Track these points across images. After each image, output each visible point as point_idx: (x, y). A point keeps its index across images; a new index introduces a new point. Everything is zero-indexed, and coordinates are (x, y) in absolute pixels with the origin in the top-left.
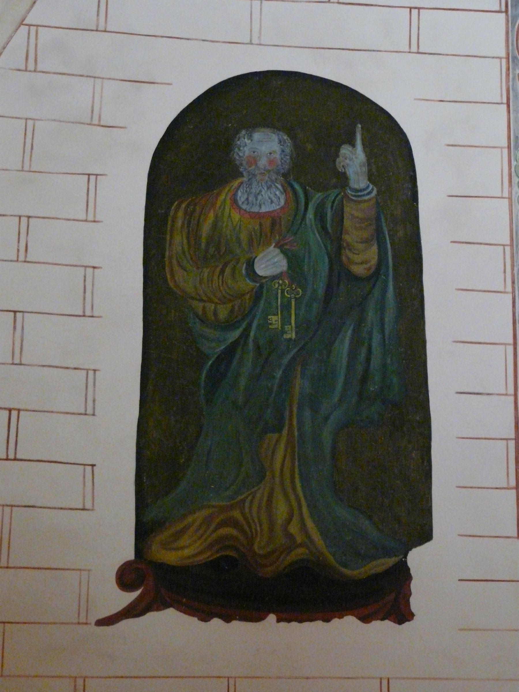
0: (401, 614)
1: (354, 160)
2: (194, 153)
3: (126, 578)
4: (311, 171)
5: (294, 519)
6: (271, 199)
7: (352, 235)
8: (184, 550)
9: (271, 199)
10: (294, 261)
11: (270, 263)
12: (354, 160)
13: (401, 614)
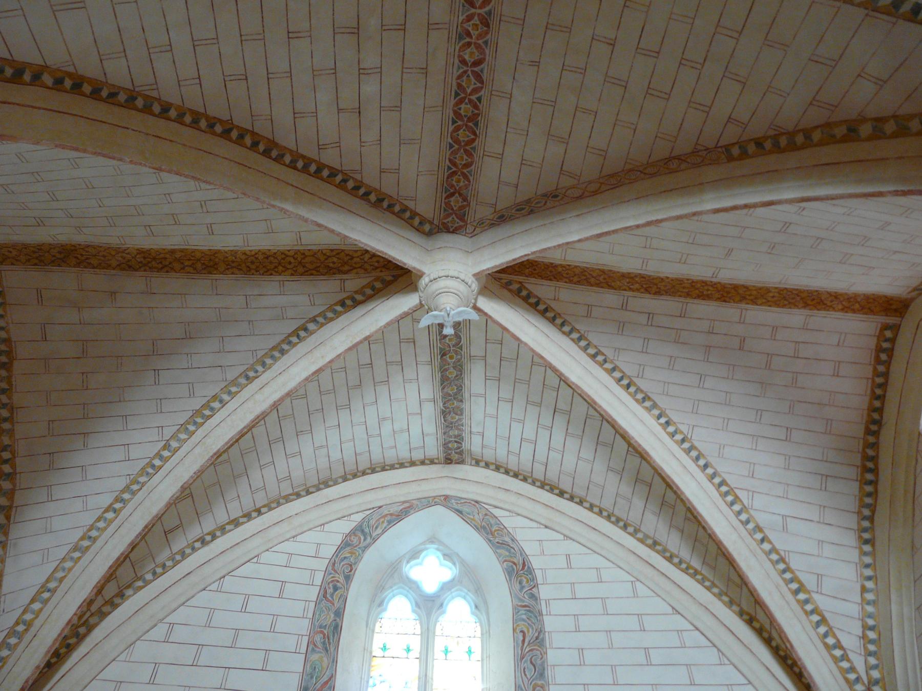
5: (528, 538)
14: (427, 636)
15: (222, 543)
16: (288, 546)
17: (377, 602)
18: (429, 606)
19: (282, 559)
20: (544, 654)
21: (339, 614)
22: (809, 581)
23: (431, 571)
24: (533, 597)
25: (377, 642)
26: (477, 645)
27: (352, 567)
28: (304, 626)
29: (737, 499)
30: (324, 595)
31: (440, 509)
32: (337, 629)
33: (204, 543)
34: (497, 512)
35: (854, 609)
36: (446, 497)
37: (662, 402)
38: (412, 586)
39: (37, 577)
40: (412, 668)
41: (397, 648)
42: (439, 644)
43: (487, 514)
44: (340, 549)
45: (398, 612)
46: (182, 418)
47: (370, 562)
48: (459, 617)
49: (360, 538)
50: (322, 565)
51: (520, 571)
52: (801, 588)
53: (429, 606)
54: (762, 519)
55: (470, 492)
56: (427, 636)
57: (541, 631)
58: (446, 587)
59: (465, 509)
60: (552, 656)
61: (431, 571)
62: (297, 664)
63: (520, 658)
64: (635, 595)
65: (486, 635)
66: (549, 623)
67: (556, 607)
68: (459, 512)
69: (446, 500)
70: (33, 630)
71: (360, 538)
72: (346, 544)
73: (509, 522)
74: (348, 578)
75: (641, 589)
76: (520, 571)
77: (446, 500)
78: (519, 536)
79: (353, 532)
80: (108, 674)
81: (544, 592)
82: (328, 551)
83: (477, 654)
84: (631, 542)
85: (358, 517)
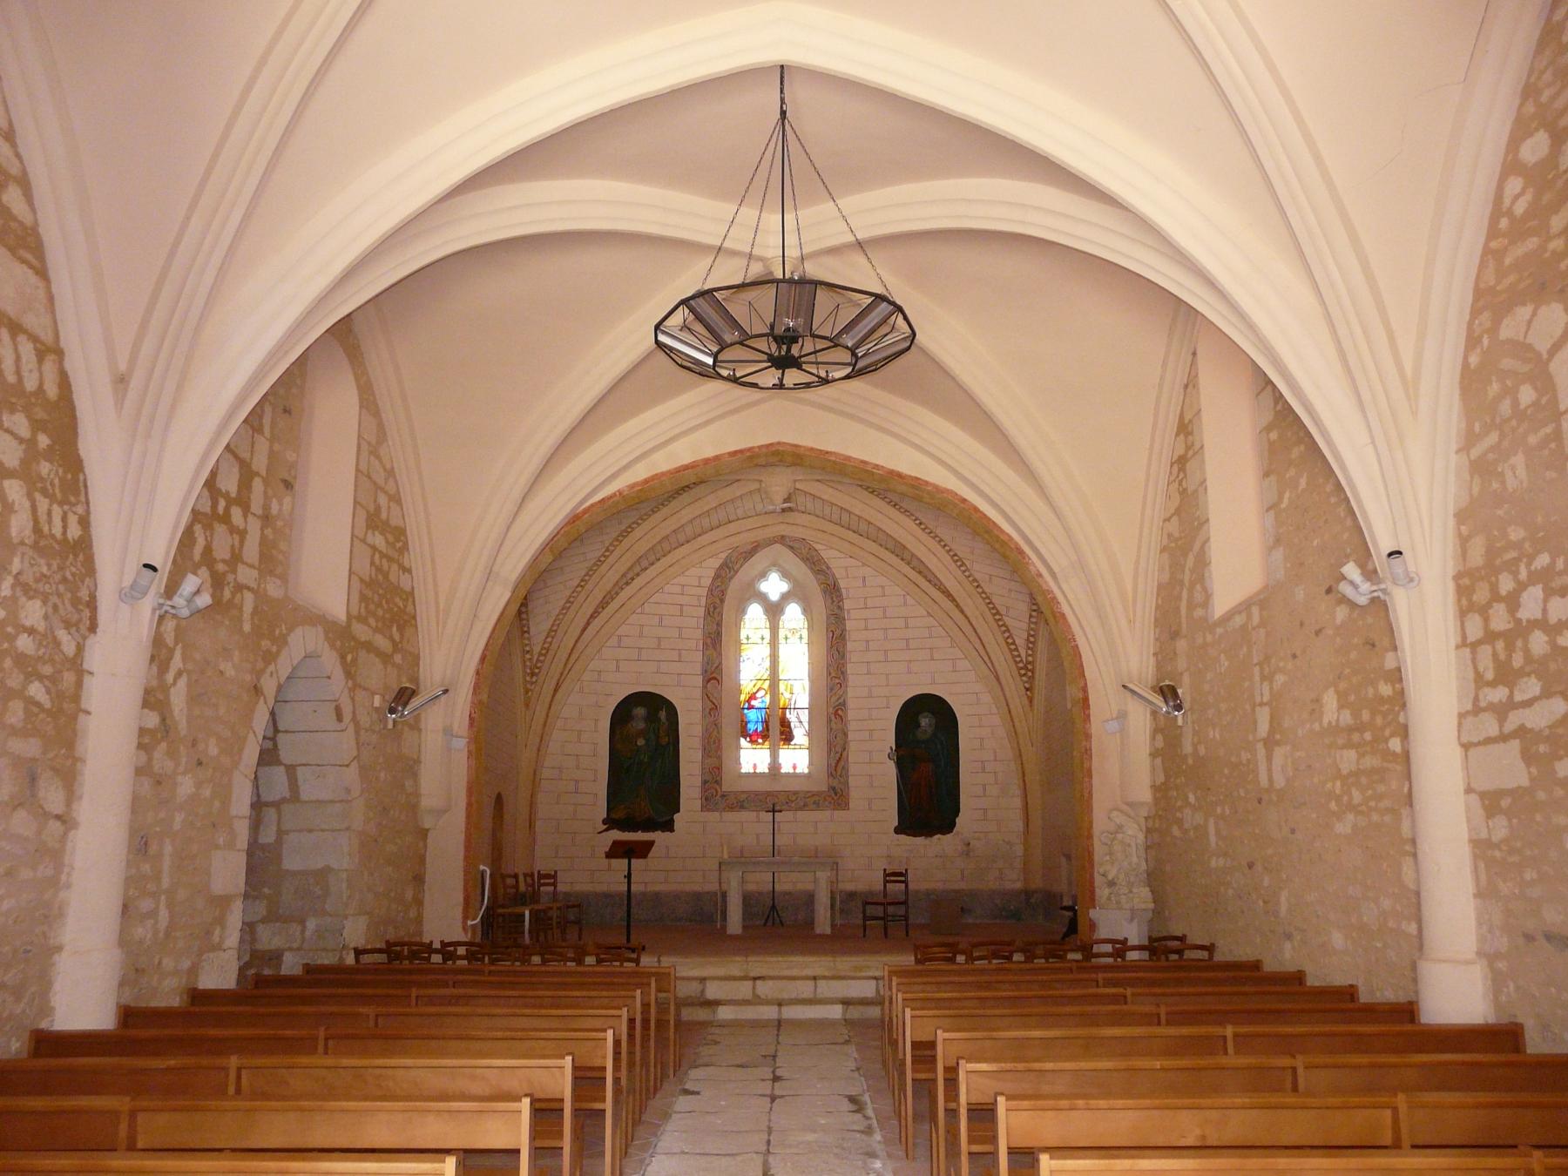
0: (672, 830)
1: (663, 715)
2: (622, 714)
3: (604, 822)
4: (652, 718)
6: (641, 725)
7: (662, 734)
8: (619, 814)
9: (641, 725)
10: (647, 740)
11: (641, 742)
12: (663, 715)
13: (672, 830)
14: (774, 629)
15: (638, 582)
16: (681, 580)
17: (741, 612)
18: (774, 611)
19: (678, 589)
20: (845, 645)
21: (719, 624)
22: (1003, 610)
23: (774, 586)
24: (839, 608)
25: (743, 636)
26: (805, 634)
27: (723, 593)
28: (699, 634)
29: (963, 564)
30: (708, 613)
31: (778, 546)
32: (719, 634)
33: (627, 584)
34: (818, 547)
35: (1025, 626)
36: (783, 537)
37: (918, 514)
38: (763, 598)
39: (546, 626)
40: (765, 650)
41: (755, 638)
42: (782, 633)
43: (811, 548)
44: (714, 579)
45: (755, 615)
46: (615, 535)
47: (734, 586)
48: (794, 615)
49: (725, 572)
50: (704, 592)
51: (832, 591)
52: (998, 613)
53: (774, 611)
54: (978, 576)
55: (799, 533)
56: (774, 629)
57: (844, 630)
58: (785, 598)
59: (796, 545)
60: (850, 646)
61: (774, 586)
62: (699, 657)
63: (831, 647)
64: (905, 604)
65: (811, 629)
66: (849, 625)
67: (854, 614)
68: (791, 548)
69: (782, 539)
70: (551, 653)
71: (725, 572)
72: (717, 576)
73: (827, 554)
74: (722, 601)
75: (910, 600)
76: (832, 591)
77: (782, 539)
78: (833, 564)
79: (721, 567)
80: (591, 667)
81: (847, 604)
82: (707, 582)
83: (805, 640)
84: (907, 570)
85: (723, 556)
